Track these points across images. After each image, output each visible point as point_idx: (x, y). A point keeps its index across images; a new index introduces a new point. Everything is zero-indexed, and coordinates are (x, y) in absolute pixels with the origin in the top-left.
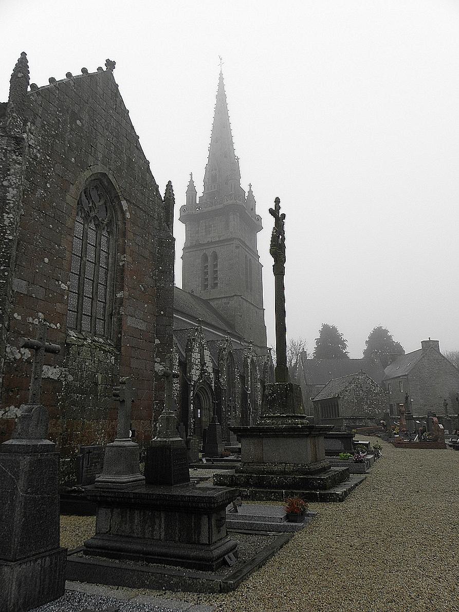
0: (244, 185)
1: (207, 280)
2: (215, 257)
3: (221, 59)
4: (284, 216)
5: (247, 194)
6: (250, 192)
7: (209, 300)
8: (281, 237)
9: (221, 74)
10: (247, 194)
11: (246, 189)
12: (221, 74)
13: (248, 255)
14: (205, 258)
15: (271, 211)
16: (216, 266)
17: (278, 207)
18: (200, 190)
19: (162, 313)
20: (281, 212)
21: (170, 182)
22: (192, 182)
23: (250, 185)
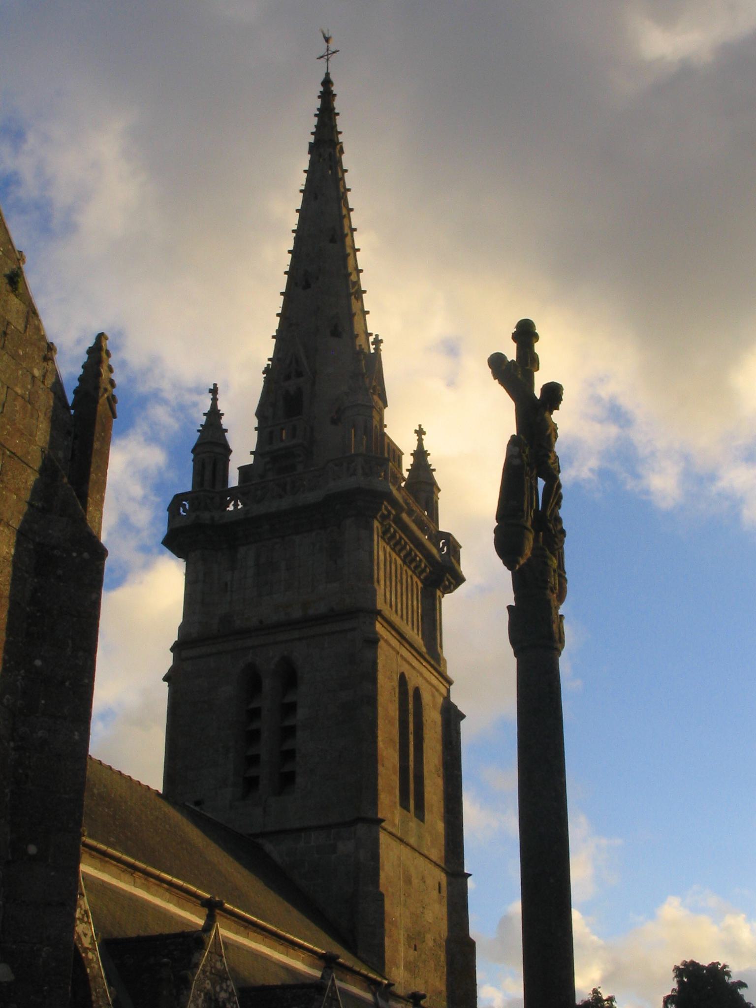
0: (399, 430)
1: (253, 760)
2: (289, 677)
3: (327, 40)
4: (553, 393)
5: (407, 462)
6: (420, 454)
7: (263, 835)
8: (541, 483)
9: (327, 83)
10: (407, 462)
11: (406, 444)
12: (327, 83)
13: (410, 674)
14: (252, 682)
15: (497, 363)
16: (290, 709)
17: (528, 359)
18: (242, 445)
19: (32, 849)
20: (540, 380)
21: (101, 337)
22: (214, 415)
23: (420, 432)
